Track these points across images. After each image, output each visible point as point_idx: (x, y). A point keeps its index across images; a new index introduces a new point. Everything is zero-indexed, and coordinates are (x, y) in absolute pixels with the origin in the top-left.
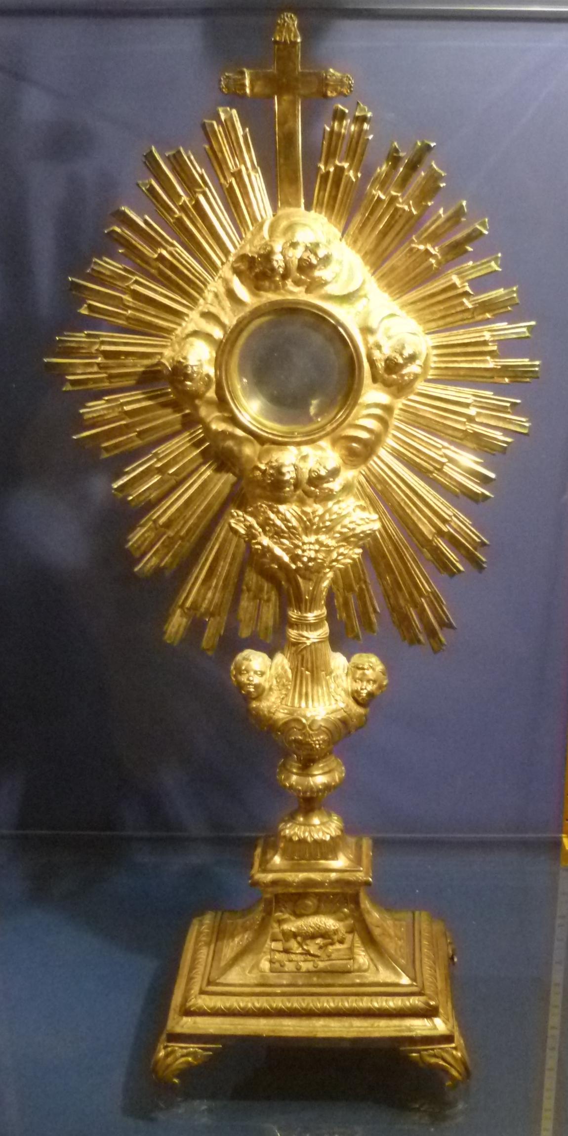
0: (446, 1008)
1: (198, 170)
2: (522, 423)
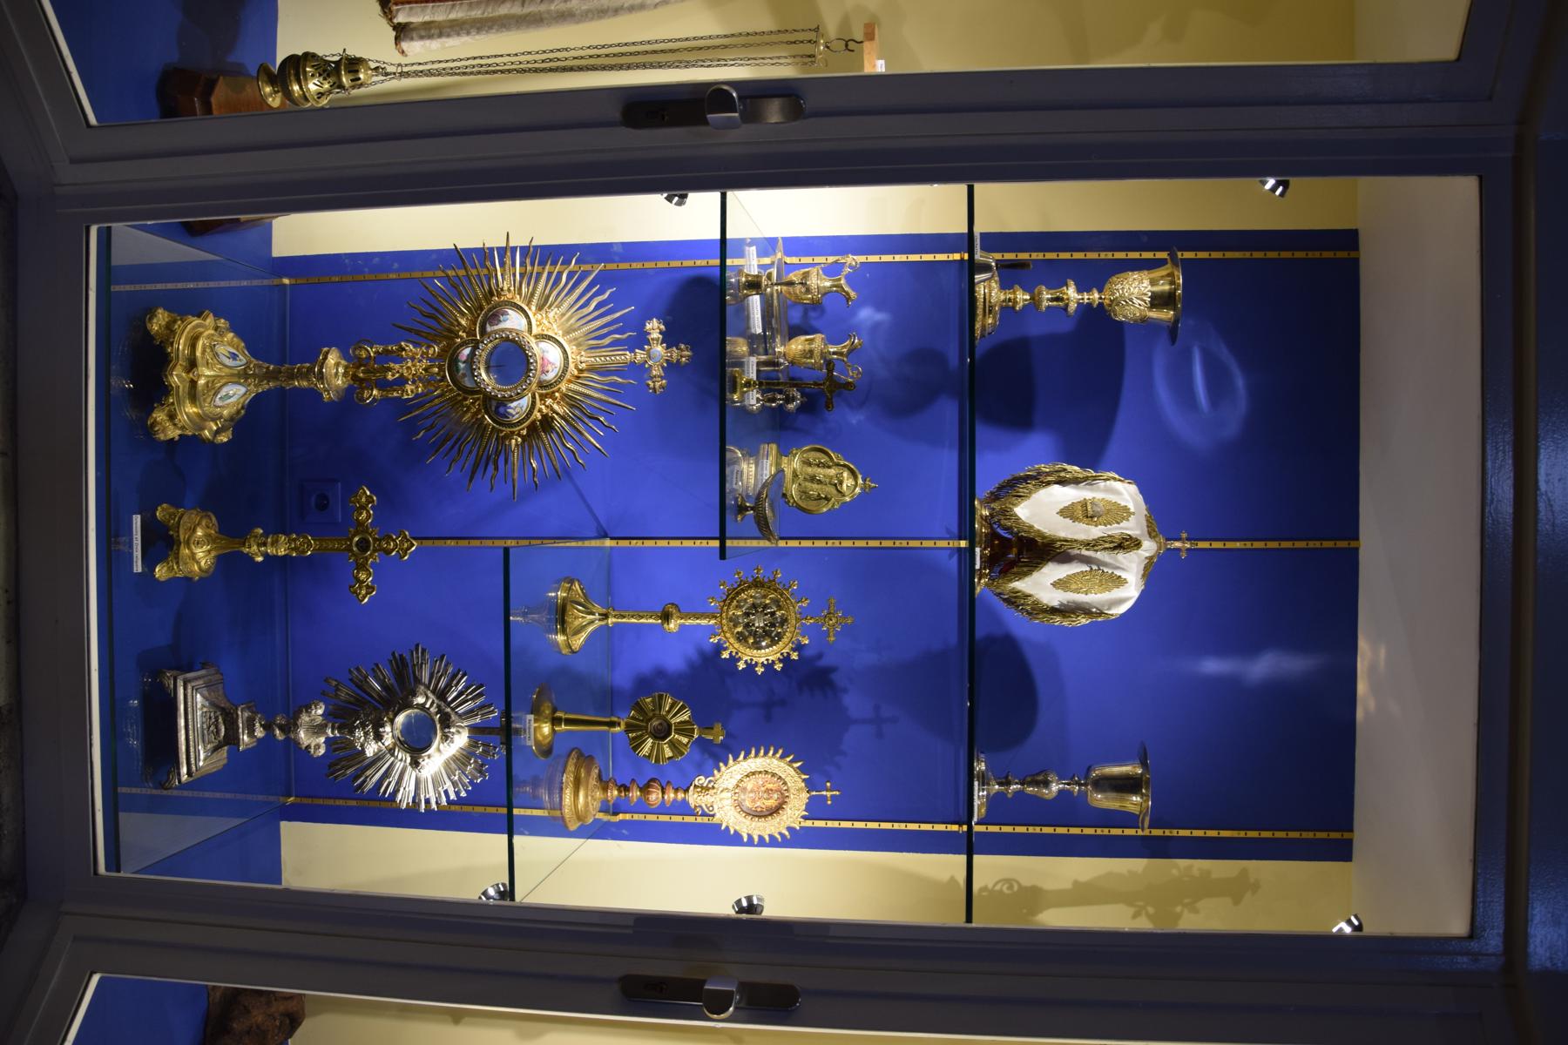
1: (478, 702)
2: (404, 806)
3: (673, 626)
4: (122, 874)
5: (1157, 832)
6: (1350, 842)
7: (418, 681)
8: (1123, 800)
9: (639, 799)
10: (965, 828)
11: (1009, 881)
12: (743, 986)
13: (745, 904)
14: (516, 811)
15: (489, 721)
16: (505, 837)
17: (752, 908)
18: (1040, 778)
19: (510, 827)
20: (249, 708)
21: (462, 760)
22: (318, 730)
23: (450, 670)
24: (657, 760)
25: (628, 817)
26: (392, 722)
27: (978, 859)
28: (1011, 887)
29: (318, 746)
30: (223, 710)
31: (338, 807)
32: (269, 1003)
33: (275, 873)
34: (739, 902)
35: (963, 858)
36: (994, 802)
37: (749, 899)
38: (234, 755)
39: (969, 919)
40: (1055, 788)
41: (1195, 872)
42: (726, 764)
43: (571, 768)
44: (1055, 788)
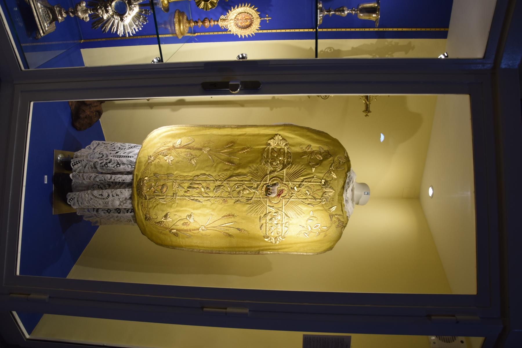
2: (121, 36)
4: (30, 69)
5: (381, 29)
6: (447, 32)
8: (370, 16)
9: (202, 25)
10: (315, 30)
11: (330, 48)
12: (242, 83)
13: (241, 56)
14: (160, 36)
16: (158, 45)
17: (243, 57)
18: (341, 9)
19: (159, 42)
20: (58, 7)
21: (139, 14)
22: (85, 12)
24: (206, 10)
25: (199, 34)
26: (111, 5)
27: (319, 41)
28: (331, 50)
29: (86, 18)
30: (49, 8)
31: (99, 42)
32: (90, 108)
33: (82, 63)
34: (239, 56)
35: (314, 41)
36: (325, 18)
37: (242, 55)
39: (316, 56)
40: (346, 12)
41: (393, 43)
42: (231, 10)
43: (177, 16)
44: (346, 12)
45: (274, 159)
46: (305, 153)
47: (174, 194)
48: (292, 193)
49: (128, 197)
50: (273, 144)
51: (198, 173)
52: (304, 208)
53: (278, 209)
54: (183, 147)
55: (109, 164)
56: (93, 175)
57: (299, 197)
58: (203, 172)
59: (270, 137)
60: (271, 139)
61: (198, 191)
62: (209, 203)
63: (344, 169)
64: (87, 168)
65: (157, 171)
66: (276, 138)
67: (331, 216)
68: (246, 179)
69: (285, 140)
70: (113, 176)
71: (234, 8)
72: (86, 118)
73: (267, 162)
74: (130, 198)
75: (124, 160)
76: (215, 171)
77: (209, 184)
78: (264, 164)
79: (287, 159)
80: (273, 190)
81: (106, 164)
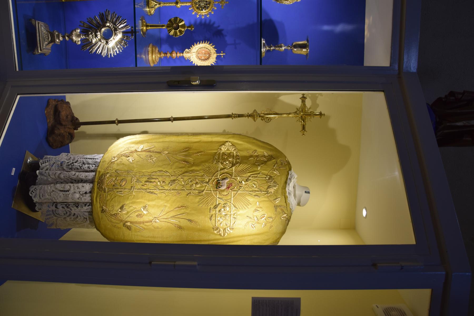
0: (42, 52)
3: (179, 5)
7: (107, 20)
8: (301, 51)
15: (128, 30)
21: (120, 42)
22: (78, 36)
23: (116, 16)
26: (100, 32)
29: (78, 41)
36: (268, 51)
38: (55, 46)
40: (283, 48)
44: (283, 48)
45: (225, 160)
46: (251, 156)
47: (132, 187)
48: (240, 187)
49: (88, 192)
50: (224, 149)
51: (156, 170)
52: (251, 199)
53: (226, 200)
54: (145, 151)
55: (74, 164)
56: (59, 172)
57: (246, 189)
58: (160, 169)
59: (221, 144)
60: (222, 145)
61: (154, 184)
62: (163, 195)
63: (286, 169)
64: (53, 167)
65: (118, 168)
66: (227, 144)
67: (276, 207)
68: (199, 175)
69: (234, 145)
70: (77, 173)
71: (196, 44)
72: (60, 135)
73: (218, 162)
74: (90, 192)
75: (90, 161)
76: (171, 168)
77: (165, 179)
78: (216, 164)
79: (236, 160)
80: (222, 183)
81: (73, 163)
